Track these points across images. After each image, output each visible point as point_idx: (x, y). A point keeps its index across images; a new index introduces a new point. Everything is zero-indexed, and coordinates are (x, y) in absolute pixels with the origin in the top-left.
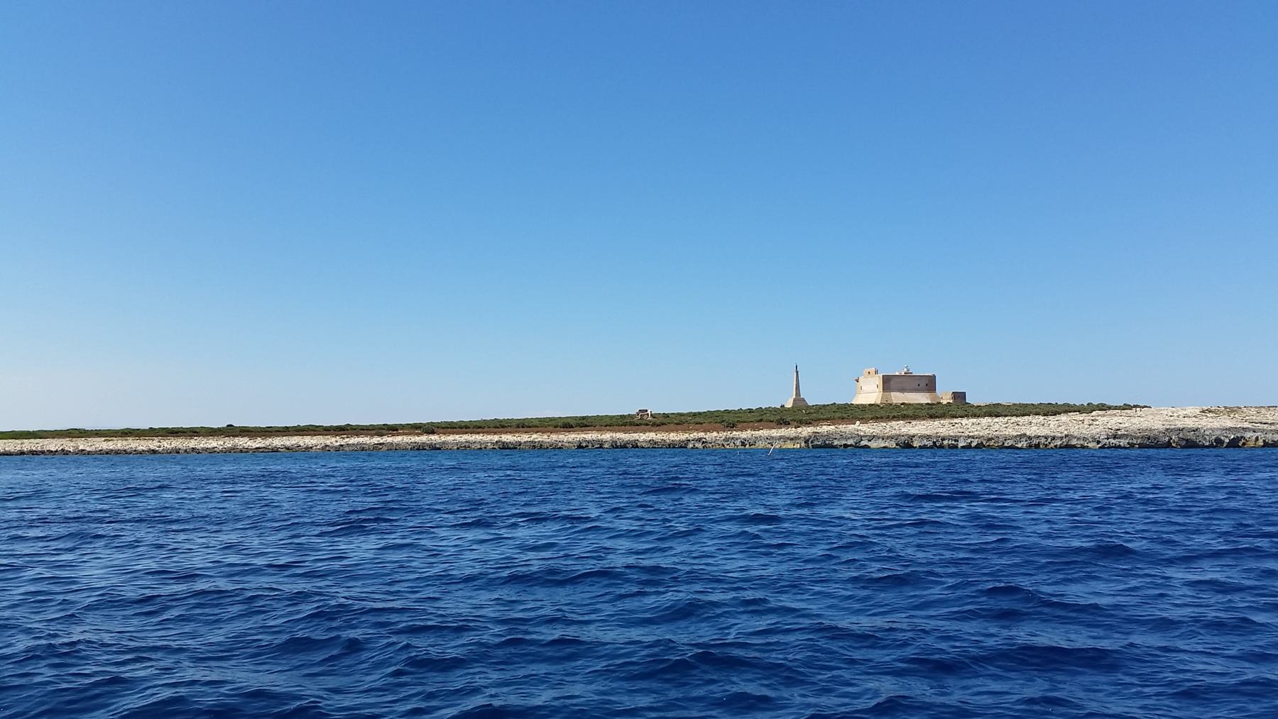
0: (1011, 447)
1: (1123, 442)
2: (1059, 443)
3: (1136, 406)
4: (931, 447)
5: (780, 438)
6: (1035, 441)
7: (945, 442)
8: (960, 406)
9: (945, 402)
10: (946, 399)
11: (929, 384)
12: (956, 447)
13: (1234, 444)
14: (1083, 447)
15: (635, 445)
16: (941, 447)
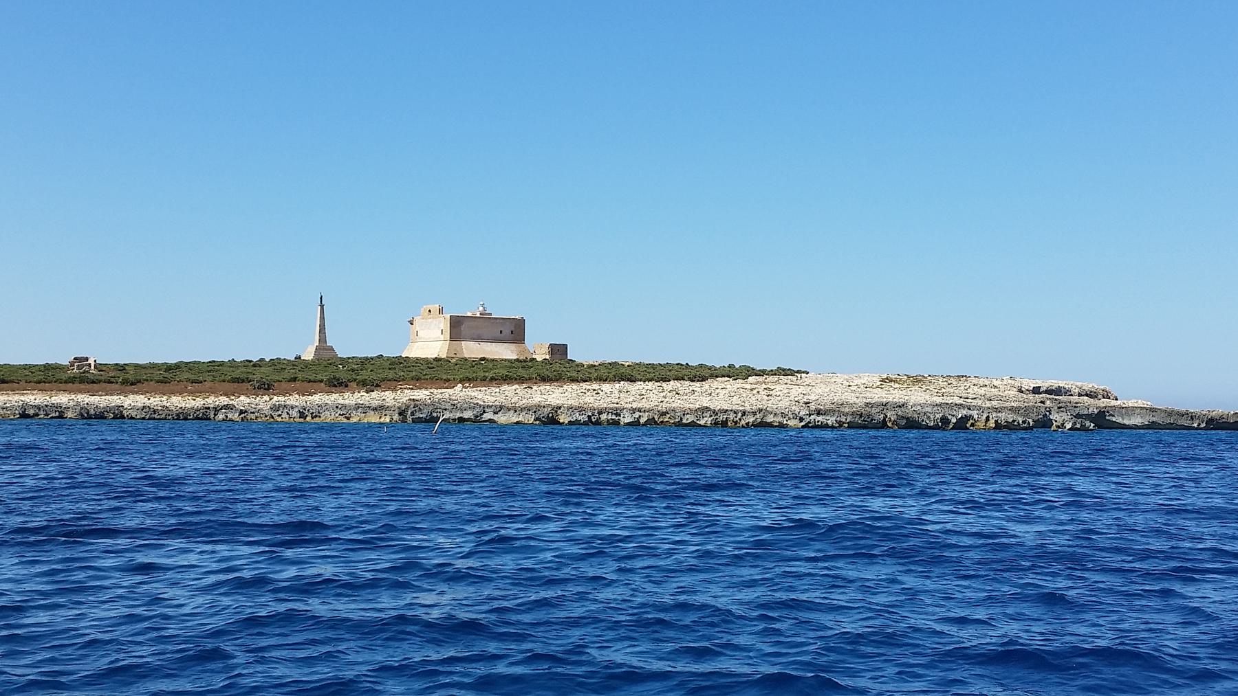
0: (693, 425)
1: (831, 420)
2: (751, 419)
3: (798, 372)
4: (585, 424)
5: (357, 407)
6: (722, 417)
7: (604, 417)
8: (557, 366)
9: (539, 358)
10: (541, 355)
11: (515, 331)
12: (616, 423)
13: (962, 424)
14: (781, 426)
15: (119, 415)
16: (598, 423)
